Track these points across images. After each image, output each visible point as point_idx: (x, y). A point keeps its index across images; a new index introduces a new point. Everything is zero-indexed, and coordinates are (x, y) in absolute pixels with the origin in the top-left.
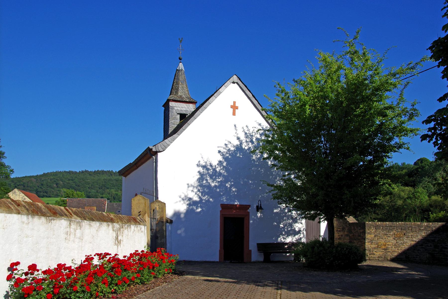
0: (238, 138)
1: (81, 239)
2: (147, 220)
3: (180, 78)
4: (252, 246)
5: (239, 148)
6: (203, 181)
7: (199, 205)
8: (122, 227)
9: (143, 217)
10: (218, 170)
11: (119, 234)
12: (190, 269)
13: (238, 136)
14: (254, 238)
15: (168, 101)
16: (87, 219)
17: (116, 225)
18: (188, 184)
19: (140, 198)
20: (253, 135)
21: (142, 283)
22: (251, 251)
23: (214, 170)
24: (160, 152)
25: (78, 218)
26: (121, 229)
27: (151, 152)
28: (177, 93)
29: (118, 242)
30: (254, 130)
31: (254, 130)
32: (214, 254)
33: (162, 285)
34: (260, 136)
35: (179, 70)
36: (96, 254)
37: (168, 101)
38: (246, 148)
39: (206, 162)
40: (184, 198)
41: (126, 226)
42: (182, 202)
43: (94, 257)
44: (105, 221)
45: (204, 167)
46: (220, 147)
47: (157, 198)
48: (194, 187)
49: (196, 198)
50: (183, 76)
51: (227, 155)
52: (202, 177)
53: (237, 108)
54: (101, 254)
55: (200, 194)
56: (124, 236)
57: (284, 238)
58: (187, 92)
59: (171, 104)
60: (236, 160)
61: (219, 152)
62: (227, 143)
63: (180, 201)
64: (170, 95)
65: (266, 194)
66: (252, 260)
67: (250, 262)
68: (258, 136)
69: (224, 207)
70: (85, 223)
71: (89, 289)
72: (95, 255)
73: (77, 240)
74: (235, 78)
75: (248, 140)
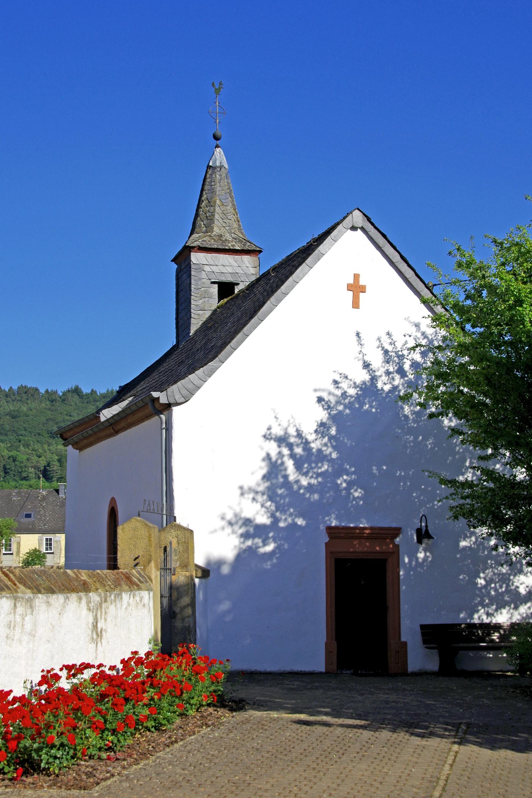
0: (366, 366)
1: (32, 635)
2: (153, 577)
3: (218, 188)
4: (409, 630)
5: (368, 389)
6: (276, 477)
7: (271, 535)
8: (106, 601)
9: (144, 570)
10: (315, 446)
11: (99, 616)
12: (252, 691)
13: (366, 358)
14: (412, 613)
15: (187, 250)
16: (43, 591)
17: (94, 597)
18: (241, 488)
19: (138, 524)
20: (403, 356)
21: (156, 729)
22: (405, 644)
23: (306, 444)
24: (178, 404)
25: (28, 591)
26: (104, 605)
27: (156, 405)
28: (209, 228)
29: (97, 633)
30: (406, 342)
31: (406, 342)
32: (312, 651)
33: (199, 732)
34: (423, 357)
35: (214, 168)
36: (64, 666)
37: (187, 250)
38: (387, 388)
39: (286, 429)
40: (234, 520)
41: (113, 597)
42: (229, 530)
43: (60, 673)
44: (73, 590)
45: (282, 440)
46: (319, 390)
47: (172, 518)
48: (257, 492)
49: (263, 519)
50: (225, 183)
51: (341, 408)
52: (274, 469)
53: (363, 289)
54: (74, 666)
55: (273, 508)
56: (109, 619)
57: (488, 614)
58: (235, 225)
59: (196, 258)
60: (360, 419)
61: (320, 400)
62: (337, 378)
63: (223, 528)
64: (192, 233)
65: (438, 503)
66: (410, 670)
67: (404, 674)
68: (417, 357)
69: (333, 532)
70: (40, 599)
71: (72, 740)
72: (61, 670)
73: (25, 638)
74: (357, 217)
75: (391, 369)
